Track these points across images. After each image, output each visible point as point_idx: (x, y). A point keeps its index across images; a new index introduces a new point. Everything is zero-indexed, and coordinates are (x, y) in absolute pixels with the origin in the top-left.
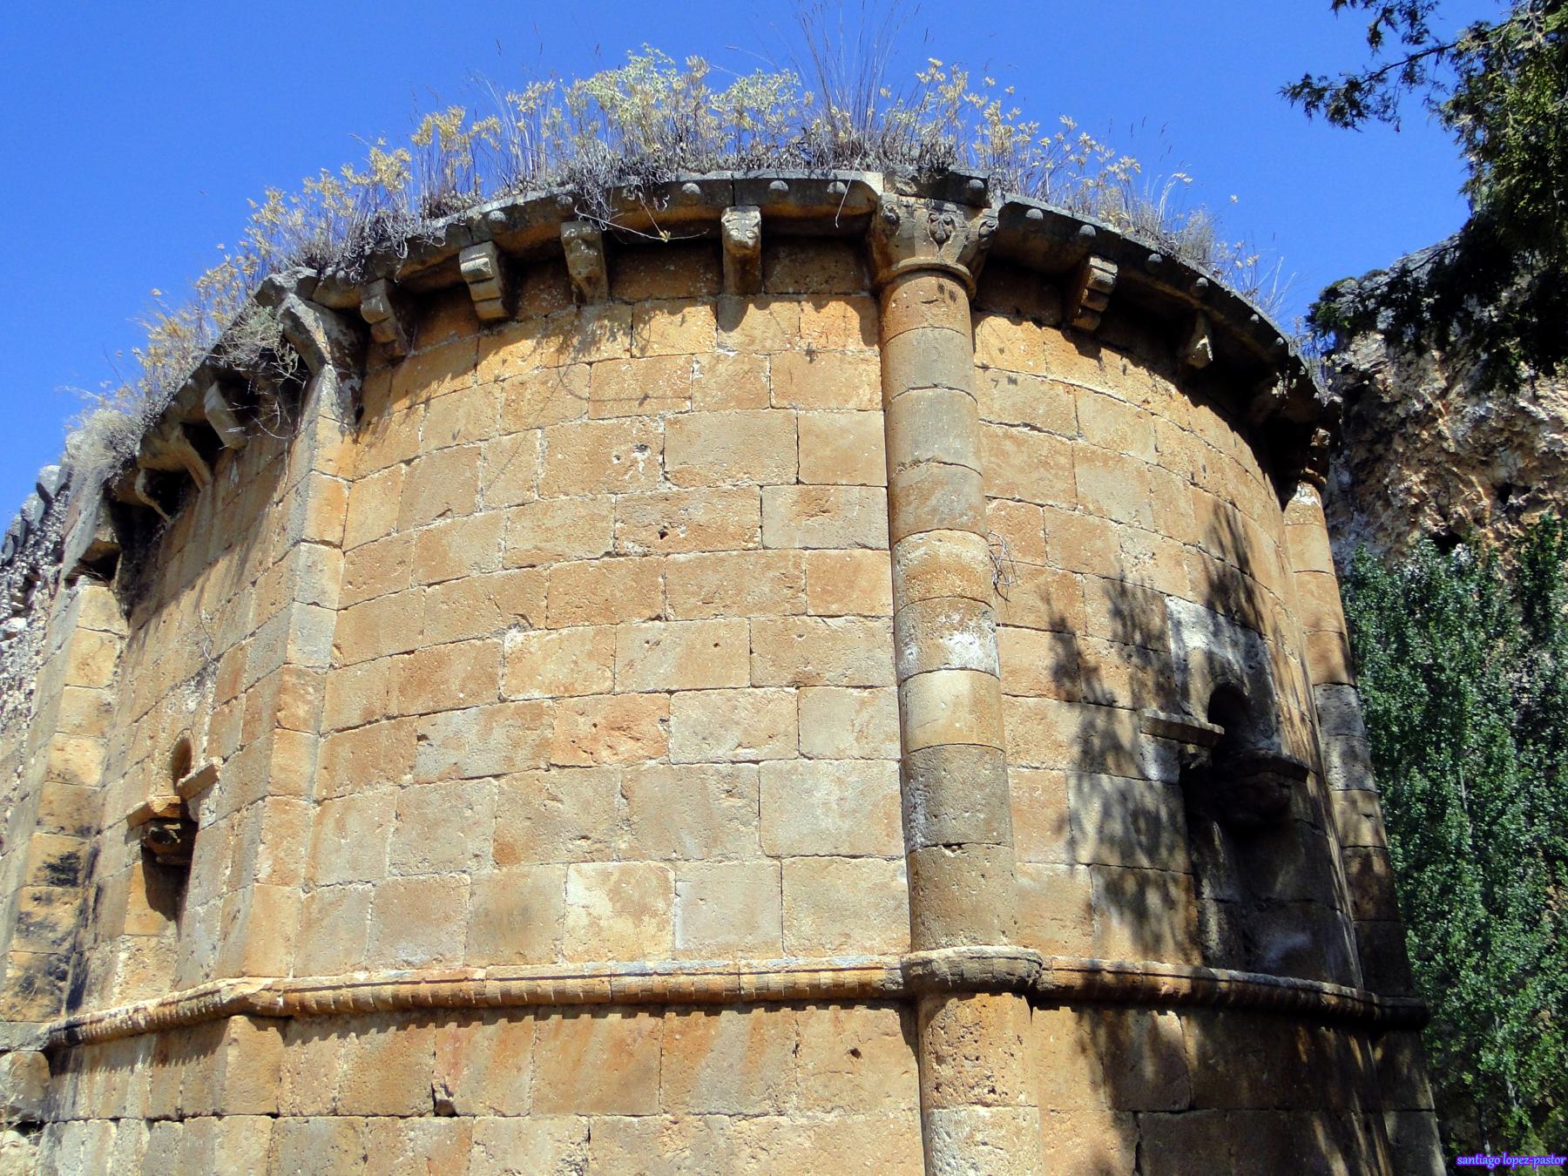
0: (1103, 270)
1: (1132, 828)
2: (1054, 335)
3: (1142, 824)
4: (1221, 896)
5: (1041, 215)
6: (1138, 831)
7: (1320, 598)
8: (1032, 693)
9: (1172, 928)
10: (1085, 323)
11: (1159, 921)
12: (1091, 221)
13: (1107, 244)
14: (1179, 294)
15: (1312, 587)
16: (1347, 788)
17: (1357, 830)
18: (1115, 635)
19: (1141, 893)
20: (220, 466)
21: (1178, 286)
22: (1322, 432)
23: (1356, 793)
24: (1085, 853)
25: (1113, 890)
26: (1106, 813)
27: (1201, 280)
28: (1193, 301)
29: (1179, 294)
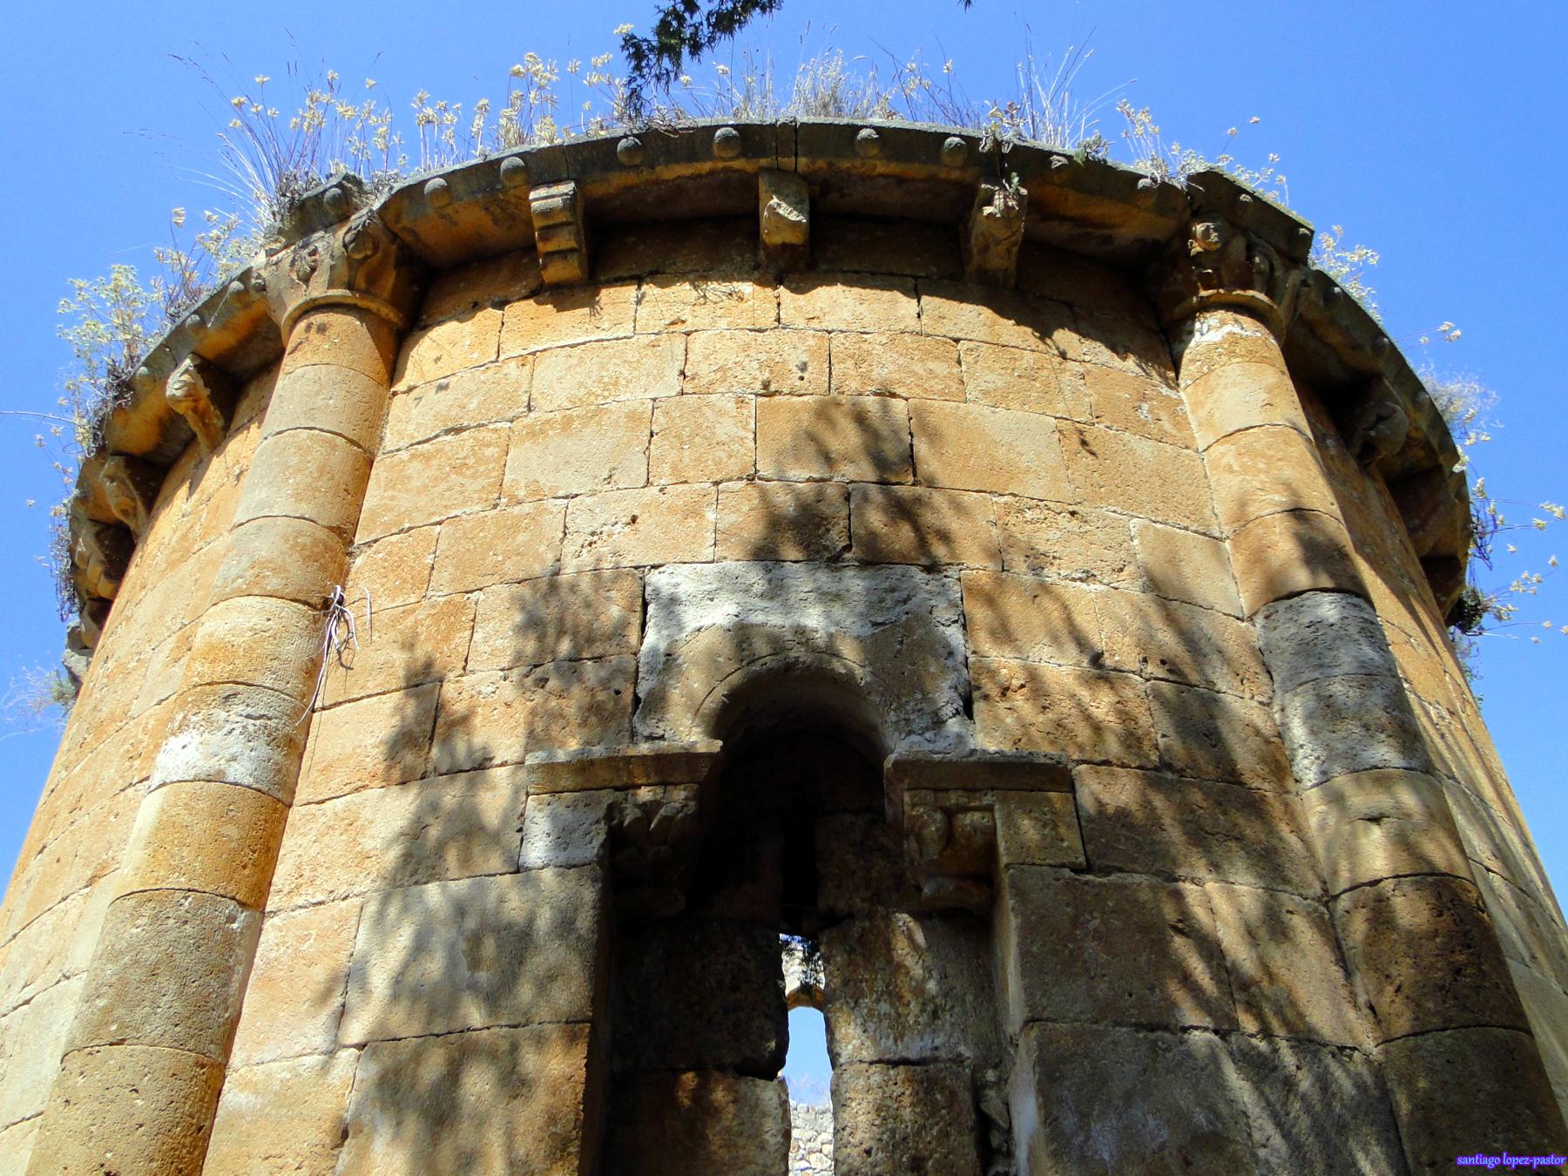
0: (547, 198)
1: (464, 962)
2: (523, 311)
3: (489, 947)
4: (902, 1051)
5: (442, 182)
6: (475, 964)
7: (1245, 469)
8: (347, 789)
9: (510, 1136)
10: (555, 272)
11: (481, 1122)
12: (508, 152)
13: (542, 166)
14: (706, 167)
15: (1230, 459)
16: (1325, 778)
17: (1353, 852)
18: (518, 658)
19: (453, 1075)
20: (979, 840)
21: (692, 157)
22: (1199, 228)
23: (1341, 780)
24: (356, 1030)
25: (392, 1089)
26: (420, 947)
27: (864, 133)
28: (736, 164)
29: (706, 167)
